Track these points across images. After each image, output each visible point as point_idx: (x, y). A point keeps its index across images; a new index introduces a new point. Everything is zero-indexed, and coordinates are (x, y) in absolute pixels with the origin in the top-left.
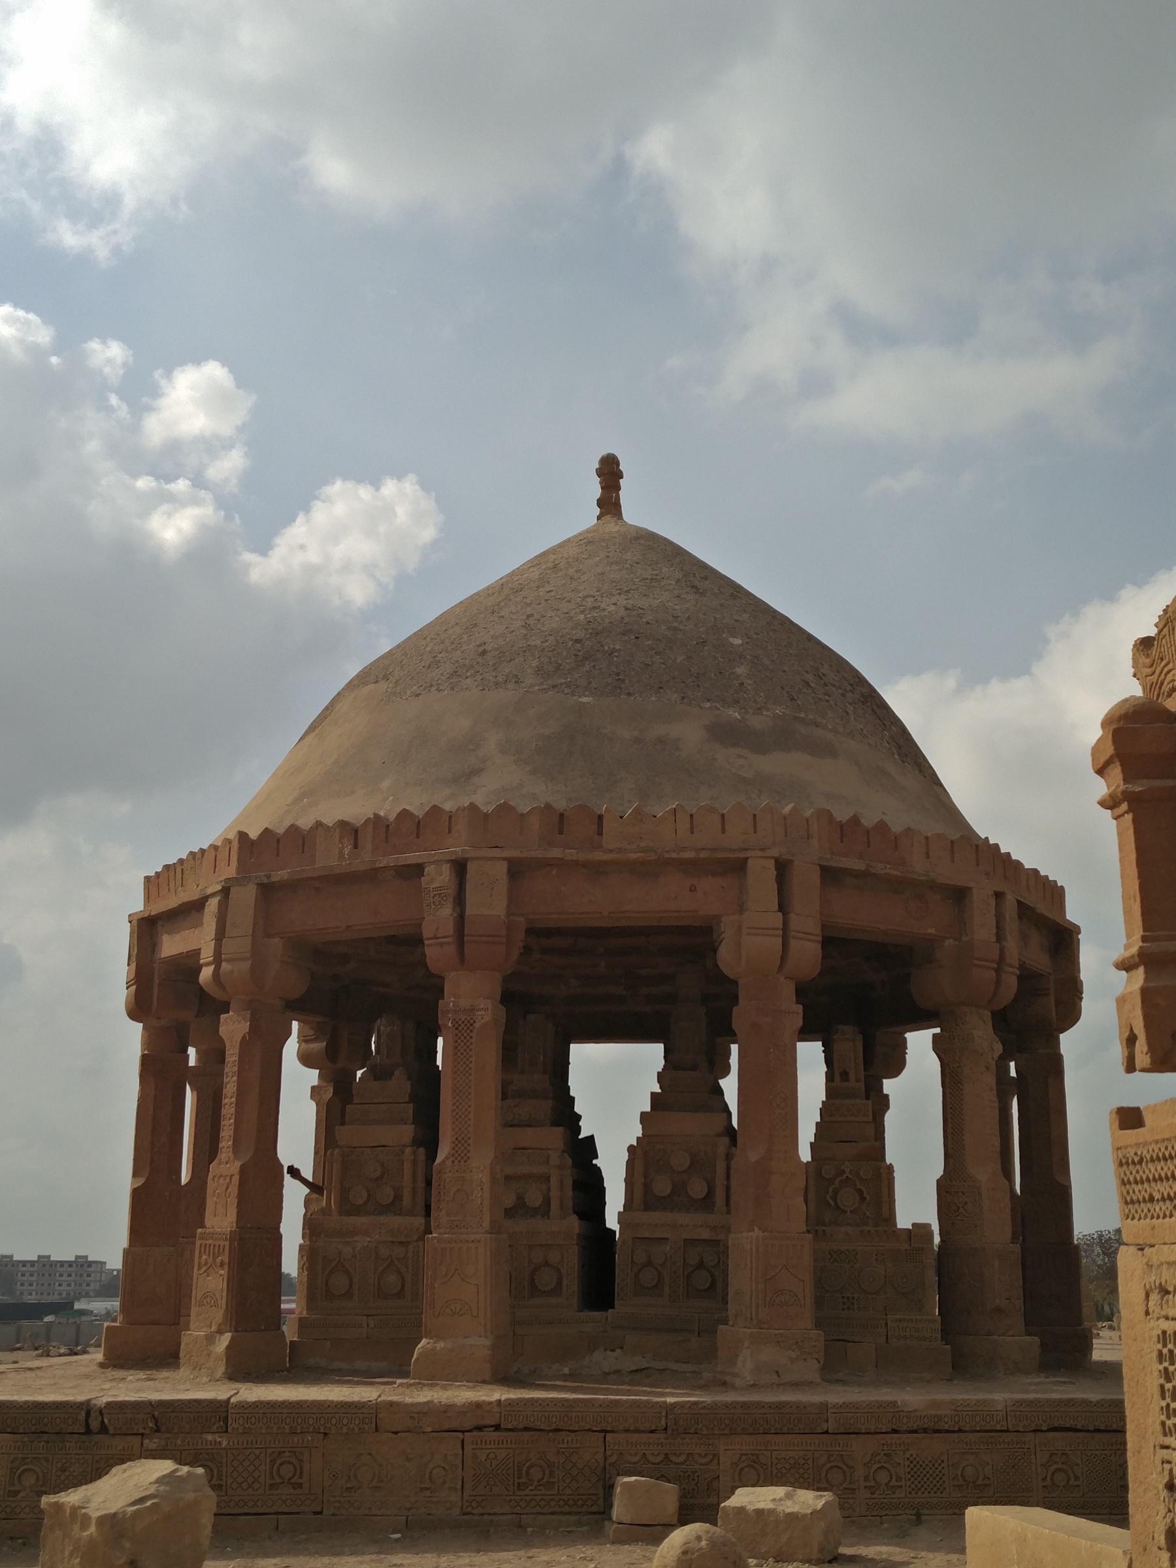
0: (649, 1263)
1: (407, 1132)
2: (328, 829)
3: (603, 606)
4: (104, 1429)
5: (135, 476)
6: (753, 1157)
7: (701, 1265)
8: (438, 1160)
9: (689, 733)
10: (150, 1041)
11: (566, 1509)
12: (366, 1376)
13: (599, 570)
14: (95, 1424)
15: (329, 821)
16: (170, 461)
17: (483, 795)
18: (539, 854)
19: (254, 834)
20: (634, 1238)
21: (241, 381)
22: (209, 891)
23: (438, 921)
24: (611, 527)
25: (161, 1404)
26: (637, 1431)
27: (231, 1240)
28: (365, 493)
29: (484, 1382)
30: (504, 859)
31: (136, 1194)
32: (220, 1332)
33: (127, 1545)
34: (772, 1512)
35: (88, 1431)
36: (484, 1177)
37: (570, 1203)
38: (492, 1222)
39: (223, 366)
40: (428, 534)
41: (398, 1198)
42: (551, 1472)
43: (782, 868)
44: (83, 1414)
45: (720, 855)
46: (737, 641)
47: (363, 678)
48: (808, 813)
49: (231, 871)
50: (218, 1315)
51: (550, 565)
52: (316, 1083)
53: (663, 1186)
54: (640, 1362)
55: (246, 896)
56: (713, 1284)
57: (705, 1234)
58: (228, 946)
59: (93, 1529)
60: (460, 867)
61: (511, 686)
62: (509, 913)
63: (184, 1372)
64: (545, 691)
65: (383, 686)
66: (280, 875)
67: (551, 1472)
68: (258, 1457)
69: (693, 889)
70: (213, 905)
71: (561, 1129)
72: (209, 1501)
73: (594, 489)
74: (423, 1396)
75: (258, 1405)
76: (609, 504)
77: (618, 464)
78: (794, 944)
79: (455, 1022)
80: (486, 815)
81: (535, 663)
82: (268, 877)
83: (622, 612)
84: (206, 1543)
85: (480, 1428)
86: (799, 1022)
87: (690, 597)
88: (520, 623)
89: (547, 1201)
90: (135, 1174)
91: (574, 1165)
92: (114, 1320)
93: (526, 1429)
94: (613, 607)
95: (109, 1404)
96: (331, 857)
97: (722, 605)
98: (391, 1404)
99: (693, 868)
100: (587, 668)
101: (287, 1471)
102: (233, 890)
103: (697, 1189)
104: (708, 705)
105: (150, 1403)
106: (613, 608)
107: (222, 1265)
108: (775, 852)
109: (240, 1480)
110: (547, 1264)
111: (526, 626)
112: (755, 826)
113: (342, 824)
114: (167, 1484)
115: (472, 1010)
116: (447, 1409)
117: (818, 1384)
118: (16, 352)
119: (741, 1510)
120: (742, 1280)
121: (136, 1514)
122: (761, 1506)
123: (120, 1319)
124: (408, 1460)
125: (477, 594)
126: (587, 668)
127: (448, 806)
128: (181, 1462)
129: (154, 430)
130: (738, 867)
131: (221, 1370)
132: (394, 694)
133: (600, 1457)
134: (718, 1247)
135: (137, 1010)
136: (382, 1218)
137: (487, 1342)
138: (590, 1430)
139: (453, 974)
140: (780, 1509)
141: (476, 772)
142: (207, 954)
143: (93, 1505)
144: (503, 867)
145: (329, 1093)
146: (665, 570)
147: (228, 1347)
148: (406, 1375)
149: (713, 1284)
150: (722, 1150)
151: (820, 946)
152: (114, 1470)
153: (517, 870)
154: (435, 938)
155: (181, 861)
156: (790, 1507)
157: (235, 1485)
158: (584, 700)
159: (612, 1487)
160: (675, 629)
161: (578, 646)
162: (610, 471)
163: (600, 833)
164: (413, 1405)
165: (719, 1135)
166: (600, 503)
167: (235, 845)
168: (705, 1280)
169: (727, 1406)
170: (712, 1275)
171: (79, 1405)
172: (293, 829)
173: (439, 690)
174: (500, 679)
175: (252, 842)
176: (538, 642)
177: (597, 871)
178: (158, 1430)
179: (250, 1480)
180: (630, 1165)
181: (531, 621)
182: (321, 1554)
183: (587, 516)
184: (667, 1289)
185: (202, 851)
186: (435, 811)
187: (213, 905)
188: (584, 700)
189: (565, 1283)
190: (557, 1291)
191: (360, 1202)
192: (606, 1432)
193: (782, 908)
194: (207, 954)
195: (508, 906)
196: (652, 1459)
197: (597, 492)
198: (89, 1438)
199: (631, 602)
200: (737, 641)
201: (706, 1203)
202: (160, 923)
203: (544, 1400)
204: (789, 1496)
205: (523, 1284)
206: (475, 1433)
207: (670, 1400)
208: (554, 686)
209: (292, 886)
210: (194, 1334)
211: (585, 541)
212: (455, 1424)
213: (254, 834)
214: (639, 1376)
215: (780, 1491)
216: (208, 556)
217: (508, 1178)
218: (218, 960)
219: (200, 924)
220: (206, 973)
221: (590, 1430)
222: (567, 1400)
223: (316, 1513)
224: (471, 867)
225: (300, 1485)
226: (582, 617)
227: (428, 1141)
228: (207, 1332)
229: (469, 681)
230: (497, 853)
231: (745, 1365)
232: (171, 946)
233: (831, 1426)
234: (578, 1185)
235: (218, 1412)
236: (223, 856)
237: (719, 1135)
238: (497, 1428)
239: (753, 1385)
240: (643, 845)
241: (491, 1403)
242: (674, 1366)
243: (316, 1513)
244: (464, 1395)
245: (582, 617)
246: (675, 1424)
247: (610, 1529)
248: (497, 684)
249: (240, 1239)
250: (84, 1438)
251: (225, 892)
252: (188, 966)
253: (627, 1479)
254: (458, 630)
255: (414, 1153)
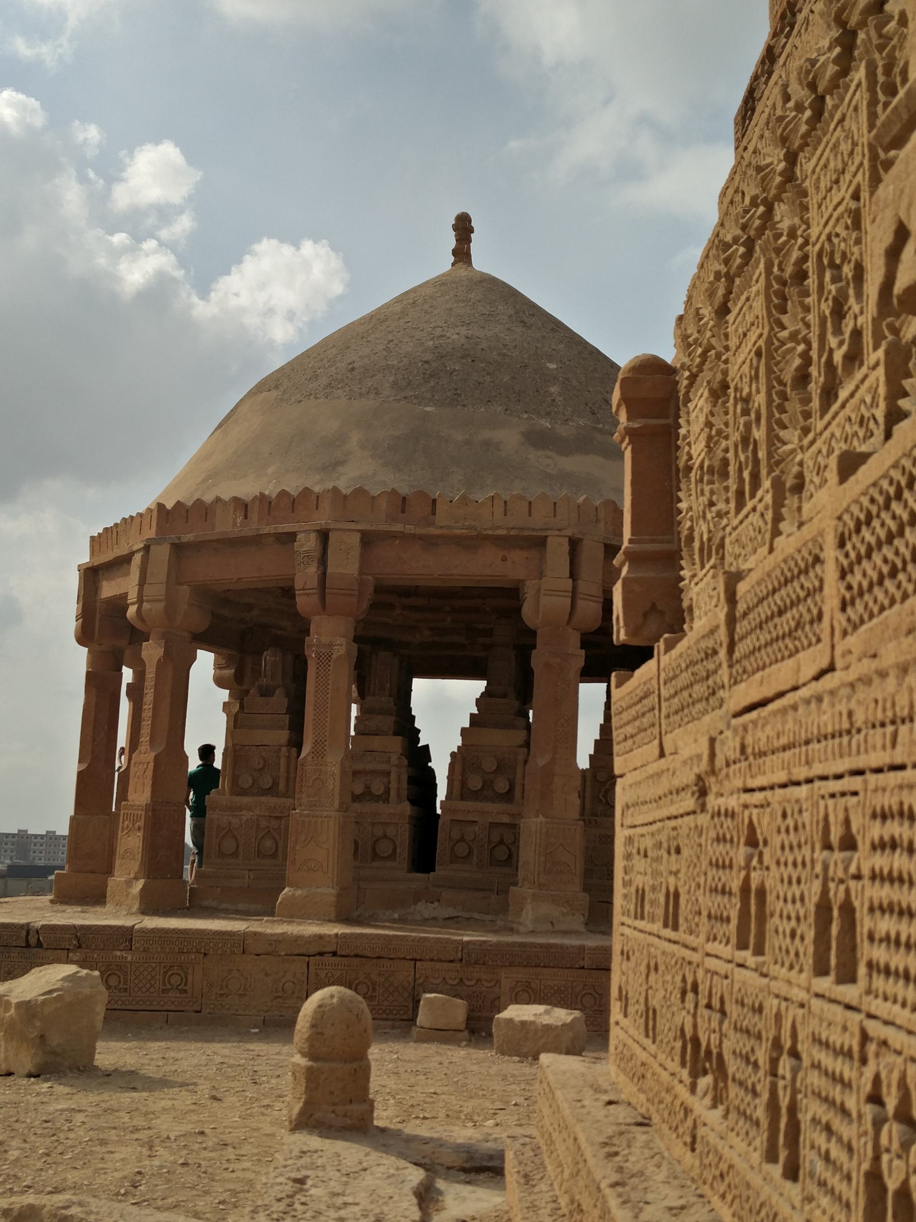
0: (462, 839)
1: (283, 735)
2: (225, 503)
3: (448, 335)
4: (39, 945)
5: (112, 233)
6: (541, 762)
7: (501, 842)
8: (302, 756)
9: (509, 437)
10: (92, 661)
11: (384, 1016)
12: (246, 914)
13: (448, 306)
14: (33, 941)
15: (226, 497)
16: (140, 224)
17: (344, 482)
18: (386, 528)
19: (169, 506)
20: (452, 820)
21: (190, 158)
22: (135, 548)
23: (306, 577)
24: (462, 272)
25: (82, 927)
26: (441, 961)
27: (146, 811)
28: (287, 250)
29: (330, 921)
30: (358, 531)
31: (81, 775)
32: (136, 878)
33: (38, 1024)
34: (532, 1023)
35: (28, 946)
36: (336, 770)
37: (405, 793)
38: (341, 804)
39: (176, 146)
40: (338, 289)
41: (275, 784)
42: (374, 989)
43: (574, 544)
44: (24, 933)
45: (526, 533)
46: (552, 366)
47: (261, 387)
48: (597, 503)
49: (151, 533)
50: (135, 866)
51: (410, 302)
52: (227, 700)
53: (475, 783)
54: (450, 912)
55: (162, 553)
56: (510, 856)
57: (506, 819)
58: (148, 590)
59: (13, 1011)
60: (324, 536)
61: (372, 396)
62: (361, 573)
63: (109, 907)
64: (399, 401)
65: (274, 394)
66: (188, 537)
67: (374, 989)
68: (154, 969)
69: (504, 559)
70: (137, 559)
71: (399, 738)
72: (102, 997)
73: (450, 241)
74: (280, 929)
75: (154, 931)
76: (462, 254)
77: (470, 221)
78: (580, 603)
79: (317, 654)
80: (345, 496)
81: (392, 379)
82: (179, 538)
83: (463, 341)
84: (99, 1025)
85: (321, 954)
86: (580, 662)
87: (518, 330)
88: (381, 347)
89: (387, 791)
90: (80, 761)
91: (409, 765)
92: (62, 868)
93: (356, 956)
94: (456, 336)
95: (43, 926)
96: (226, 525)
97: (544, 337)
98: (255, 933)
99: (506, 542)
100: (432, 384)
101: (176, 980)
102: (152, 548)
103: (501, 786)
104: (525, 416)
105: (74, 926)
106: (456, 336)
107: (139, 829)
108: (569, 532)
109: (140, 985)
110: (385, 837)
111: (387, 349)
112: (555, 511)
113: (236, 499)
114: (70, 981)
115: (331, 645)
116: (297, 939)
117: (582, 933)
118: (15, 130)
119: (511, 1021)
120: (529, 854)
121: (44, 1002)
122: (525, 1018)
123: (67, 868)
124: (267, 975)
125: (352, 323)
126: (432, 384)
127: (317, 489)
128: (82, 967)
129: (121, 198)
130: (539, 543)
131: (136, 907)
132: (282, 400)
133: (411, 979)
134: (513, 827)
135: (84, 637)
136: (263, 799)
137: (334, 892)
138: (404, 958)
139: (317, 618)
140: (539, 1021)
141: (342, 463)
142: (132, 596)
143: (14, 994)
144: (357, 537)
145: (236, 708)
146: (501, 307)
147: (142, 890)
148: (272, 914)
149: (510, 856)
150: (521, 758)
151: (600, 606)
152: (33, 971)
153: (368, 540)
154: (303, 589)
155: (116, 525)
156: (546, 1020)
157: (136, 989)
158: (428, 409)
159: (419, 1001)
160: (504, 355)
161: (427, 366)
162: (463, 227)
163: (434, 513)
164: (272, 935)
165: (520, 746)
166: (455, 252)
167: (155, 513)
168: (503, 853)
169: (508, 944)
170: (510, 850)
171: (22, 926)
172: (199, 503)
173: (316, 398)
174: (364, 390)
175: (168, 512)
176: (395, 362)
177: (430, 542)
178: (80, 947)
179: (148, 986)
180: (452, 766)
181: (391, 345)
182: (197, 1041)
183: (444, 263)
184: (475, 859)
185: (132, 517)
186: (307, 492)
187: (137, 559)
188: (428, 409)
189: (398, 851)
190: (392, 856)
191: (246, 786)
192: (415, 960)
193: (573, 575)
194: (132, 596)
195: (361, 568)
196: (451, 982)
197: (452, 243)
198: (22, 948)
199: (471, 332)
200: (552, 366)
201: (508, 796)
202: (101, 573)
203: (371, 935)
204: (547, 1012)
205: (364, 851)
206: (318, 958)
207: (466, 939)
208: (405, 398)
209: (198, 546)
210: (118, 879)
211: (440, 283)
212: (303, 950)
213: (169, 506)
214: (451, 921)
215: (540, 1008)
216: (157, 293)
217: (355, 773)
218: (140, 600)
219: (128, 574)
220: (132, 611)
221: (404, 958)
222: (388, 936)
223: (196, 1012)
224: (332, 536)
225: (185, 991)
226: (431, 343)
227: (297, 743)
228: (127, 879)
229: (340, 391)
230: (352, 526)
231: (528, 915)
232: (108, 589)
233: (586, 963)
234: (412, 780)
235: (125, 936)
236: (146, 522)
237: (520, 746)
238: (334, 954)
239: (532, 932)
240: (467, 523)
241: (330, 936)
242: (477, 916)
243: (196, 1012)
244: (311, 929)
245: (431, 343)
246: (469, 957)
247: (415, 1031)
248: (361, 394)
249: (153, 810)
250: (25, 950)
251: (147, 548)
252: (119, 605)
253: (428, 995)
254: (334, 351)
255: (289, 752)
